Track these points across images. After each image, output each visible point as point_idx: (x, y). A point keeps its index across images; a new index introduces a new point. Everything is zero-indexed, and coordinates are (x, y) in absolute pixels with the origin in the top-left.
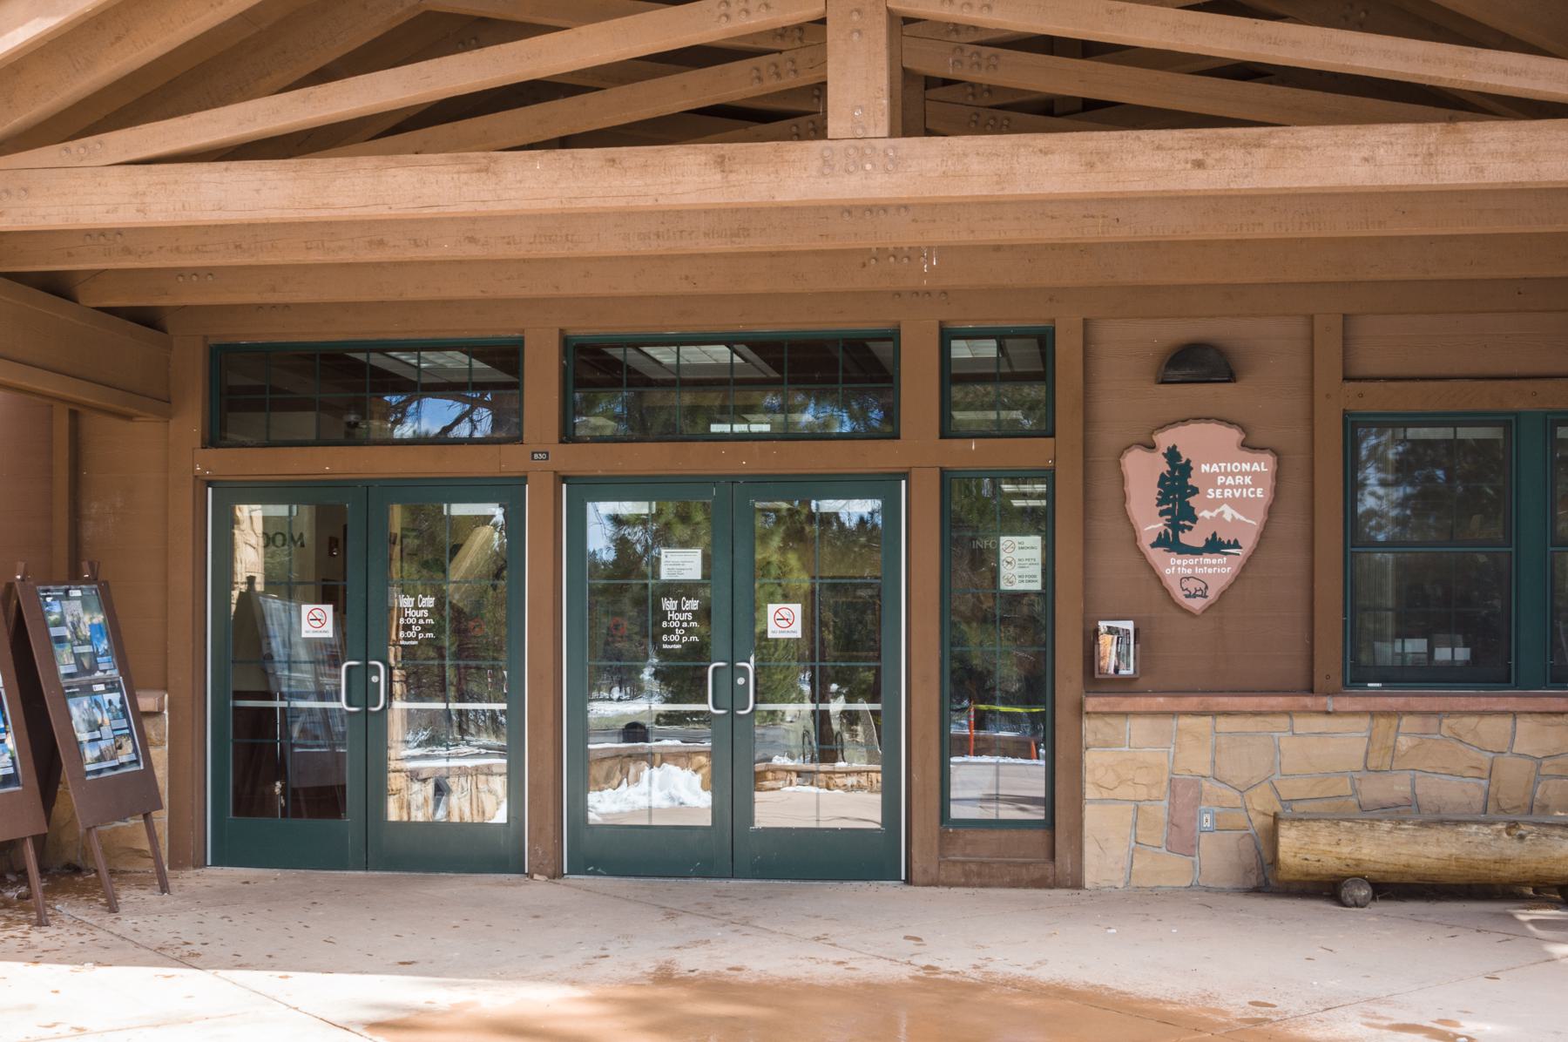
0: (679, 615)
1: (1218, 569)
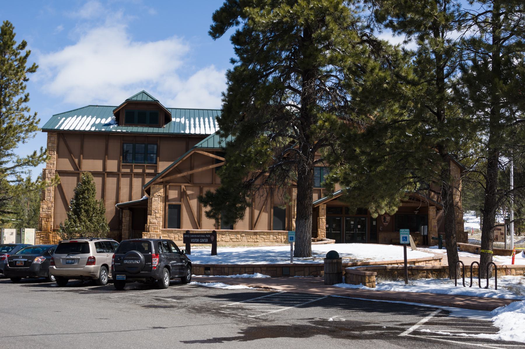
0: (352, 226)
1: (387, 224)
